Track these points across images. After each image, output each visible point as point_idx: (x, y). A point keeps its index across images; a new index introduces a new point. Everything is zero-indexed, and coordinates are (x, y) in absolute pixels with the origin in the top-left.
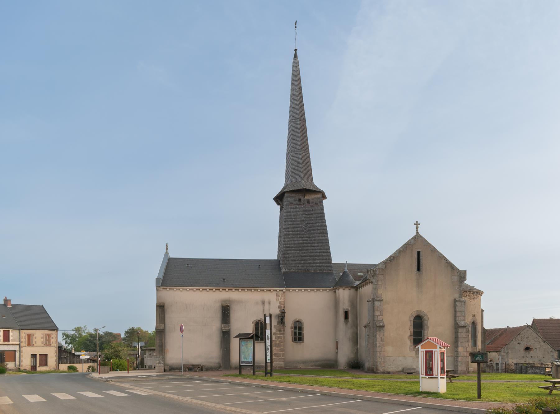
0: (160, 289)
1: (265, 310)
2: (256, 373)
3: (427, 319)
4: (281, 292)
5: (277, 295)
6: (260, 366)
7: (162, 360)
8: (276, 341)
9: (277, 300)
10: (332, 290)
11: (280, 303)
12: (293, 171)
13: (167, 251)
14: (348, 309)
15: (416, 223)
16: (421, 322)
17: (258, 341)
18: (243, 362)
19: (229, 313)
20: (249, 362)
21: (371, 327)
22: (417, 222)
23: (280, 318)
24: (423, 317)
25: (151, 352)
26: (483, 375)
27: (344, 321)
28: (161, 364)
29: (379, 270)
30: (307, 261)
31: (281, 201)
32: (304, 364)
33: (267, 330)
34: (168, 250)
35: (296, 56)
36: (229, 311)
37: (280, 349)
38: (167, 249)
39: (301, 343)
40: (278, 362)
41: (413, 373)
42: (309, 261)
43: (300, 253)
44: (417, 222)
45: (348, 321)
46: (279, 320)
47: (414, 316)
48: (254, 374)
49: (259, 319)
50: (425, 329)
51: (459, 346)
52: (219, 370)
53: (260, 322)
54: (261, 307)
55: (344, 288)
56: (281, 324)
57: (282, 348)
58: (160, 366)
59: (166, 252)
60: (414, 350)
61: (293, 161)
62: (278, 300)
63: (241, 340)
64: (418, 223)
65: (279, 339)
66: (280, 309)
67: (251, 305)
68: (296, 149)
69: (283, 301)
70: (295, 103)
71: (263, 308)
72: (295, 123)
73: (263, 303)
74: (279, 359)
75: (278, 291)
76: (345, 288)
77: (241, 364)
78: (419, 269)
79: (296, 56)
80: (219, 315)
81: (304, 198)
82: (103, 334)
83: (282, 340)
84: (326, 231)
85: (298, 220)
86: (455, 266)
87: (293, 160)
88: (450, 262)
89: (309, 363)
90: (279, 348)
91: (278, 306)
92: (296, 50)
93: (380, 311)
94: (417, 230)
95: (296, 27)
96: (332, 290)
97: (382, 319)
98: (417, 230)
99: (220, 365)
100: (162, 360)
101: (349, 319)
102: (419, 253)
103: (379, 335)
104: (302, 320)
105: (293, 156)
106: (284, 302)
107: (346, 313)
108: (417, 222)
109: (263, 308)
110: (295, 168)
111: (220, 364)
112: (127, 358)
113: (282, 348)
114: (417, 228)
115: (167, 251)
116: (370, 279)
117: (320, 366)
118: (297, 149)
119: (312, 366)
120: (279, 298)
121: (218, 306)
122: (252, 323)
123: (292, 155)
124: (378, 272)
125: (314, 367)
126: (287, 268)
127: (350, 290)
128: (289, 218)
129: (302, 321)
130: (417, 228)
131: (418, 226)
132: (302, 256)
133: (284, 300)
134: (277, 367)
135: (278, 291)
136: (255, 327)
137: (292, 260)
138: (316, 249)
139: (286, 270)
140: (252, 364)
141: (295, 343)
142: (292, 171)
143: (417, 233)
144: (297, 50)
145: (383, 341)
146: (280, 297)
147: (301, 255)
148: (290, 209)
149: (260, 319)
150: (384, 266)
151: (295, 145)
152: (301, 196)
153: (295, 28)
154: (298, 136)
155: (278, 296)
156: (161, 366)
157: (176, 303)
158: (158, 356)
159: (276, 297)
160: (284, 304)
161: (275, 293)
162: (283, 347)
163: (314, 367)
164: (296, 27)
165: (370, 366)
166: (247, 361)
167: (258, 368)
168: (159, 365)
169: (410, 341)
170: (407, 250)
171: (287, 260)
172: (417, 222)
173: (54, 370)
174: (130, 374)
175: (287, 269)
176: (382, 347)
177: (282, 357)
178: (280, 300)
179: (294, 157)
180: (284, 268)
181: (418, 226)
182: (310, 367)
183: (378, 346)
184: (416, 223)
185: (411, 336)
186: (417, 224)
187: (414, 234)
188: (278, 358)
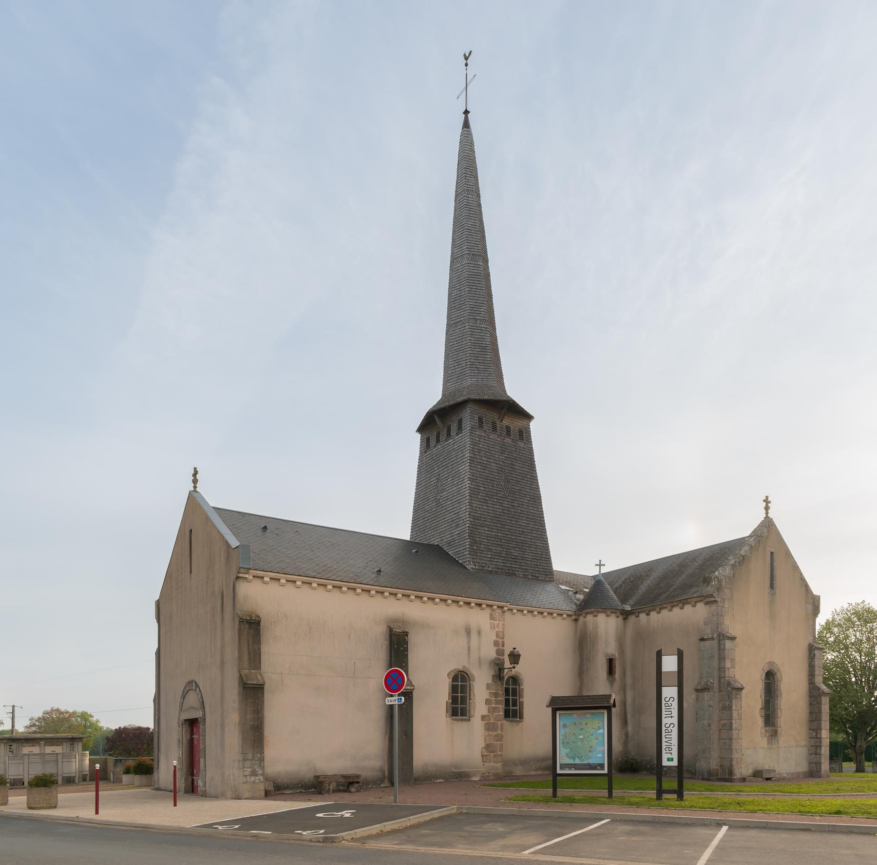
0: (247, 576)
1: (472, 648)
2: (615, 792)
3: (779, 679)
4: (499, 611)
5: (492, 618)
6: (462, 772)
7: (260, 766)
8: (490, 718)
9: (491, 628)
10: (571, 616)
11: (497, 636)
12: (474, 361)
13: (195, 487)
14: (614, 655)
16: (458, 691)
17: (458, 718)
18: (563, 766)
19: (406, 650)
20: (602, 766)
21: (716, 690)
22: (767, 497)
23: (497, 668)
24: (776, 674)
25: (14, 746)
27: (608, 679)
28: (257, 775)
29: (726, 579)
30: (512, 553)
31: (442, 421)
32: (523, 766)
33: (663, 688)
34: (197, 485)
35: (466, 125)
36: (407, 647)
37: (496, 736)
38: (195, 481)
39: (519, 722)
40: (492, 764)
41: (773, 779)
42: (515, 554)
43: (499, 534)
44: (767, 497)
45: (615, 679)
46: (495, 672)
47: (766, 671)
48: (610, 795)
49: (461, 668)
50: (777, 697)
51: (823, 728)
52: (382, 786)
53: (461, 674)
54: (463, 641)
55: (609, 613)
56: (498, 680)
57: (499, 732)
58: (254, 782)
59: (193, 489)
60: (765, 736)
61: (473, 342)
62: (493, 627)
63: (558, 713)
65: (495, 714)
66: (496, 648)
67: (446, 634)
68: (478, 318)
69: (501, 630)
70: (473, 221)
71: (469, 643)
72: (474, 263)
73: (468, 632)
74: (494, 756)
75: (495, 607)
76: (612, 613)
77: (559, 771)
78: (772, 586)
79: (466, 125)
80: (382, 654)
81: (502, 422)
83: (499, 715)
84: (539, 497)
85: (492, 464)
86: (809, 586)
87: (473, 339)
88: (804, 578)
89: (532, 763)
90: (494, 733)
91: (494, 641)
93: (732, 659)
94: (767, 513)
95: (466, 65)
96: (571, 616)
97: (734, 676)
98: (767, 513)
99: (384, 775)
100: (260, 766)
101: (616, 675)
102: (772, 553)
103: (736, 707)
104: (521, 674)
105: (473, 330)
106: (503, 633)
107: (611, 662)
109: (469, 643)
110: (477, 355)
111: (385, 772)
113: (499, 732)
114: (767, 508)
115: (195, 487)
116: (714, 594)
118: (481, 318)
119: (536, 770)
120: (494, 624)
121: (380, 631)
122: (448, 675)
123: (469, 327)
124: (724, 583)
125: (539, 772)
126: (479, 562)
127: (618, 617)
128: (478, 457)
129: (521, 677)
130: (767, 508)
132: (503, 541)
133: (504, 630)
134: (491, 774)
135: (495, 607)
137: (486, 547)
138: (525, 531)
139: (475, 565)
140: (606, 771)
141: (509, 721)
142: (472, 361)
143: (767, 517)
145: (740, 715)
146: (496, 622)
147: (500, 539)
148: (478, 439)
149: (463, 668)
150: (732, 572)
151: (475, 309)
152: (496, 417)
154: (482, 291)
155: (492, 619)
156: (257, 781)
157: (286, 616)
158: (250, 756)
159: (489, 621)
160: (503, 638)
161: (488, 611)
162: (501, 731)
163: (539, 772)
164: (466, 65)
165: (715, 768)
166: (585, 765)
167: (457, 777)
168: (253, 778)
169: (761, 718)
170: (759, 546)
171: (477, 547)
174: (110, 814)
175: (477, 564)
176: (739, 730)
177: (499, 753)
178: (497, 629)
179: (475, 333)
180: (473, 562)
181: (769, 505)
182: (533, 773)
183: (734, 728)
185: (762, 708)
186: (767, 501)
187: (761, 517)
188: (492, 755)
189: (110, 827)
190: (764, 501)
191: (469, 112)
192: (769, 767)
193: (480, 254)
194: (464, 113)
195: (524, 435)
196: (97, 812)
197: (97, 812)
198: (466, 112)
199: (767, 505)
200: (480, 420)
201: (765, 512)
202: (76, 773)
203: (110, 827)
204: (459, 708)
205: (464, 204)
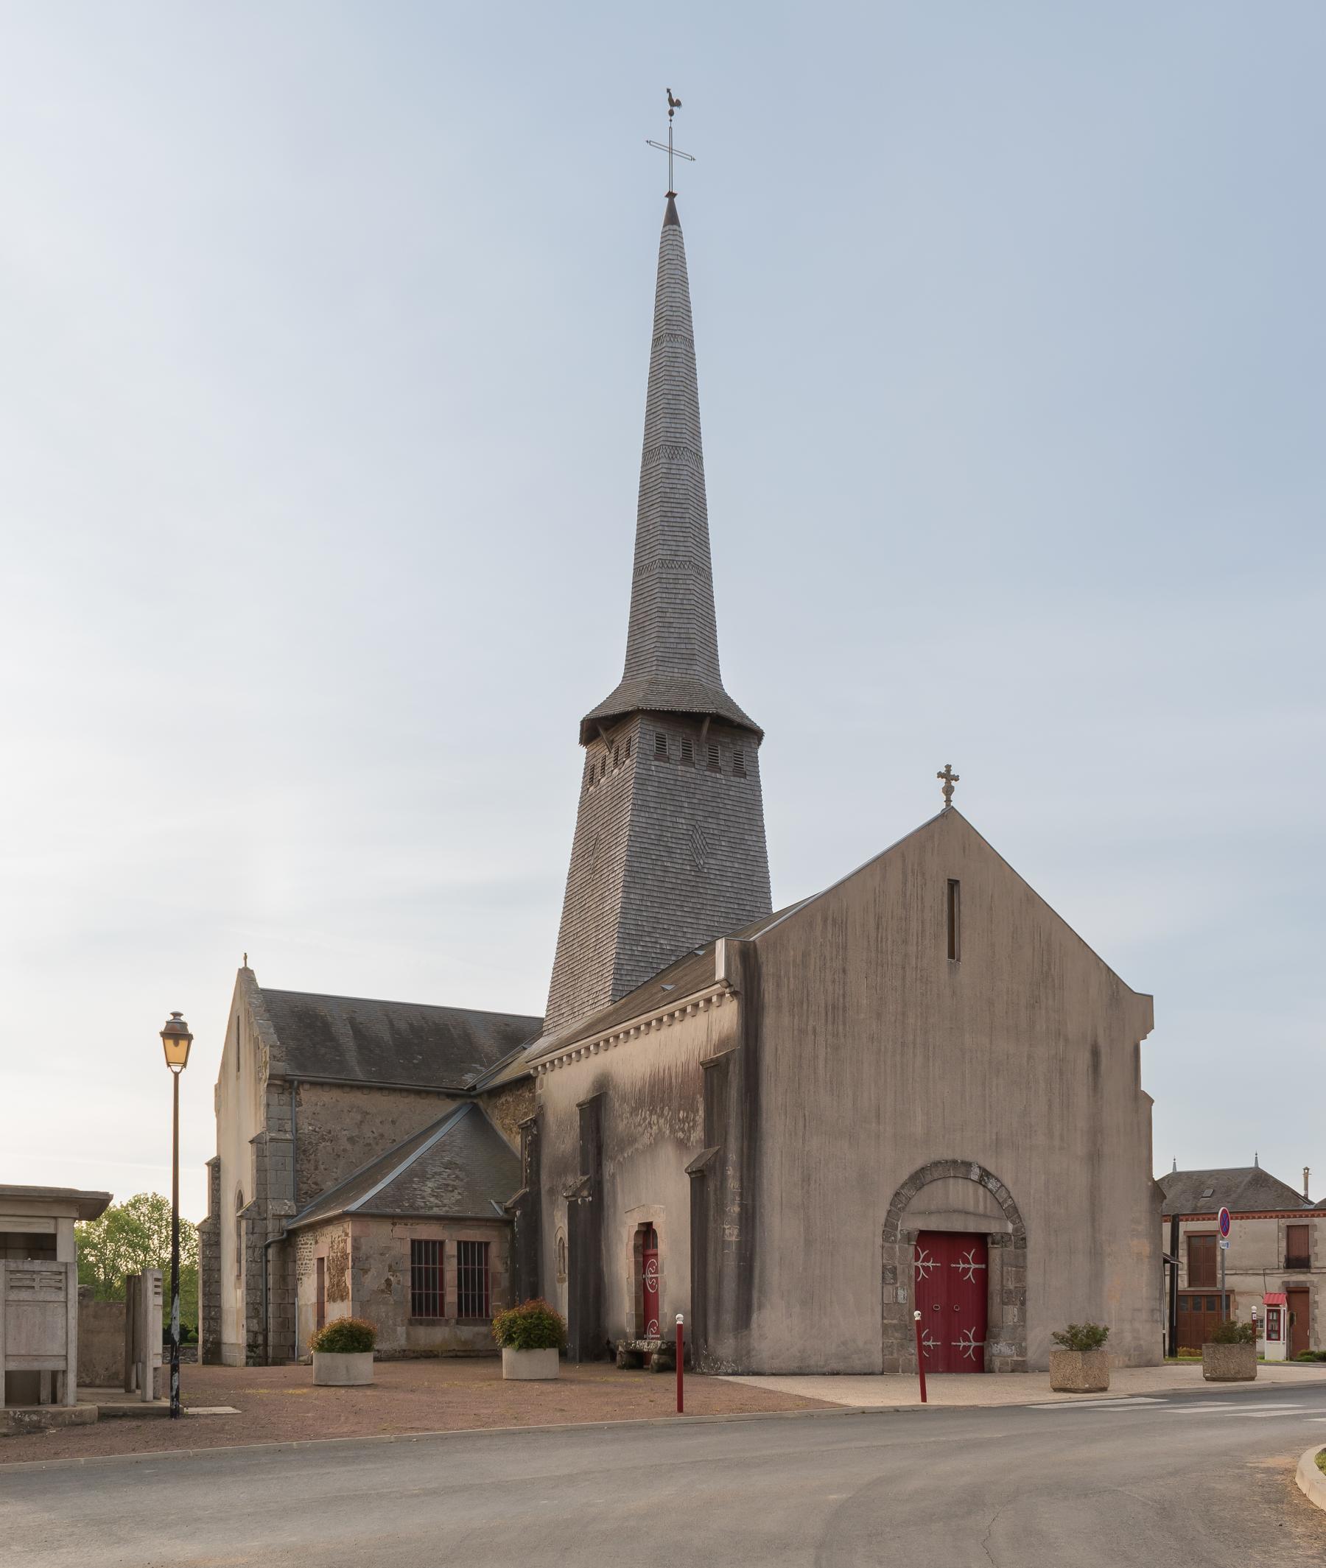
15: (943, 770)
26: (929, 1379)
35: (672, 217)
64: (952, 773)
79: (672, 217)
82: (387, 1037)
92: (671, 195)
94: (948, 801)
98: (948, 801)
108: (948, 767)
112: (421, 1054)
114: (948, 791)
117: (1096, 1041)
130: (948, 791)
131: (953, 783)
136: (37, 1374)
144: (675, 195)
153: (669, 118)
172: (948, 767)
173: (244, 1223)
181: (953, 783)
184: (943, 770)
186: (948, 776)
187: (938, 807)
189: (1045, 1407)
190: (940, 775)
191: (675, 195)
192: (1224, 1374)
193: (685, 445)
194: (667, 196)
195: (746, 770)
196: (924, 1399)
197: (924, 1399)
198: (671, 195)
199: (948, 782)
200: (661, 741)
201: (944, 798)
202: (66, 1357)
203: (1045, 1407)
204: (451, 1249)
205: (663, 355)
